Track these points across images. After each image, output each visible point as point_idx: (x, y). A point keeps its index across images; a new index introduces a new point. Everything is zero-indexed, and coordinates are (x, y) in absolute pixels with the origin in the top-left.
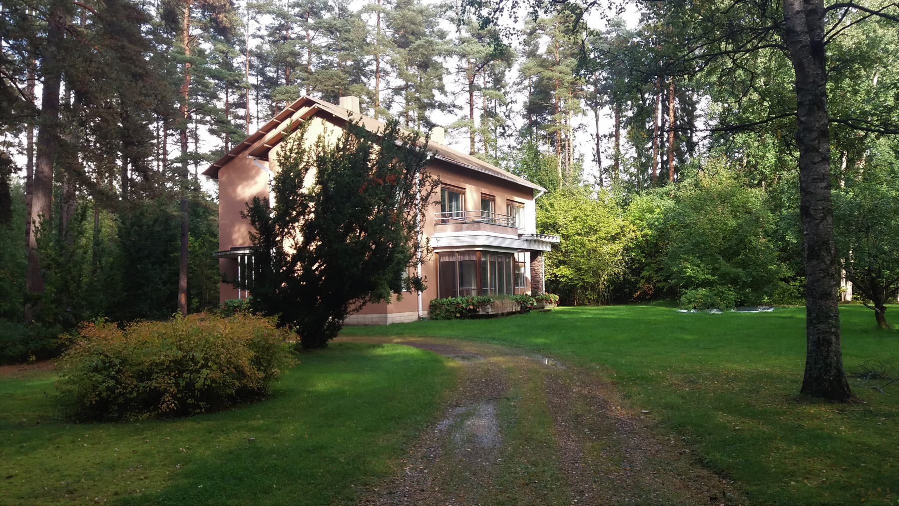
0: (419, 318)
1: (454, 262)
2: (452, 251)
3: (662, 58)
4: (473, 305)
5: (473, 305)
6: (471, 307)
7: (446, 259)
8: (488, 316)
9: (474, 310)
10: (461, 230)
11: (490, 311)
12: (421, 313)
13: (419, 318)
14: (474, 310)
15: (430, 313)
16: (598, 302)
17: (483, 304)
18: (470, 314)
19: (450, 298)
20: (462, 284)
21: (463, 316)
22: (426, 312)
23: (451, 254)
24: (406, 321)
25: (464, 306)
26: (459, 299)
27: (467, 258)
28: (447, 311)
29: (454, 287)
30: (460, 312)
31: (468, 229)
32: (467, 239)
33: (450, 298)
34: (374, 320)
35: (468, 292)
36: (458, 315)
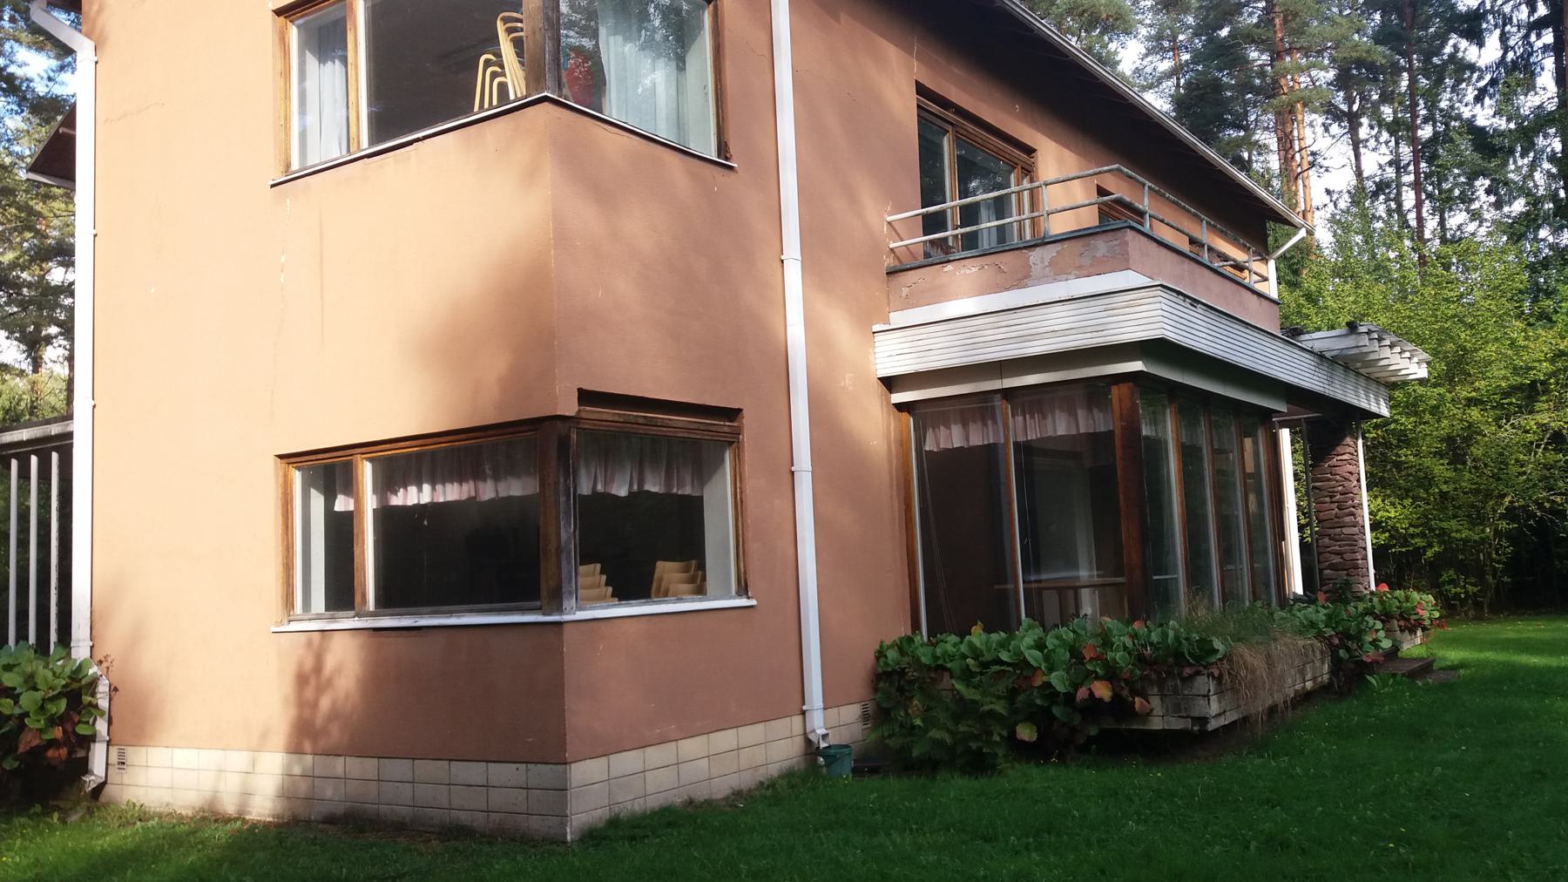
0: (811, 750)
1: (990, 451)
2: (981, 391)
3: (828, 765)
4: (1112, 675)
5: (1112, 675)
6: (1103, 691)
7: (952, 437)
8: (1193, 741)
9: (1120, 708)
10: (1021, 279)
11: (1216, 710)
12: (818, 723)
13: (811, 750)
14: (1120, 708)
15: (879, 715)
16: (1478, 606)
17: (1175, 666)
18: (1096, 731)
19: (977, 636)
20: (1033, 561)
21: (1053, 746)
22: (851, 712)
23: (977, 408)
24: (720, 788)
25: (1058, 680)
26: (1027, 639)
27: (1060, 426)
28: (963, 709)
29: (1001, 572)
30: (1040, 717)
31: (1059, 272)
32: (1060, 318)
33: (977, 636)
34: (497, 799)
35: (1068, 594)
36: (1026, 733)
